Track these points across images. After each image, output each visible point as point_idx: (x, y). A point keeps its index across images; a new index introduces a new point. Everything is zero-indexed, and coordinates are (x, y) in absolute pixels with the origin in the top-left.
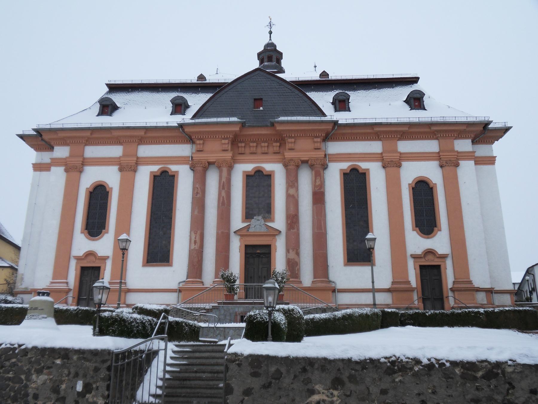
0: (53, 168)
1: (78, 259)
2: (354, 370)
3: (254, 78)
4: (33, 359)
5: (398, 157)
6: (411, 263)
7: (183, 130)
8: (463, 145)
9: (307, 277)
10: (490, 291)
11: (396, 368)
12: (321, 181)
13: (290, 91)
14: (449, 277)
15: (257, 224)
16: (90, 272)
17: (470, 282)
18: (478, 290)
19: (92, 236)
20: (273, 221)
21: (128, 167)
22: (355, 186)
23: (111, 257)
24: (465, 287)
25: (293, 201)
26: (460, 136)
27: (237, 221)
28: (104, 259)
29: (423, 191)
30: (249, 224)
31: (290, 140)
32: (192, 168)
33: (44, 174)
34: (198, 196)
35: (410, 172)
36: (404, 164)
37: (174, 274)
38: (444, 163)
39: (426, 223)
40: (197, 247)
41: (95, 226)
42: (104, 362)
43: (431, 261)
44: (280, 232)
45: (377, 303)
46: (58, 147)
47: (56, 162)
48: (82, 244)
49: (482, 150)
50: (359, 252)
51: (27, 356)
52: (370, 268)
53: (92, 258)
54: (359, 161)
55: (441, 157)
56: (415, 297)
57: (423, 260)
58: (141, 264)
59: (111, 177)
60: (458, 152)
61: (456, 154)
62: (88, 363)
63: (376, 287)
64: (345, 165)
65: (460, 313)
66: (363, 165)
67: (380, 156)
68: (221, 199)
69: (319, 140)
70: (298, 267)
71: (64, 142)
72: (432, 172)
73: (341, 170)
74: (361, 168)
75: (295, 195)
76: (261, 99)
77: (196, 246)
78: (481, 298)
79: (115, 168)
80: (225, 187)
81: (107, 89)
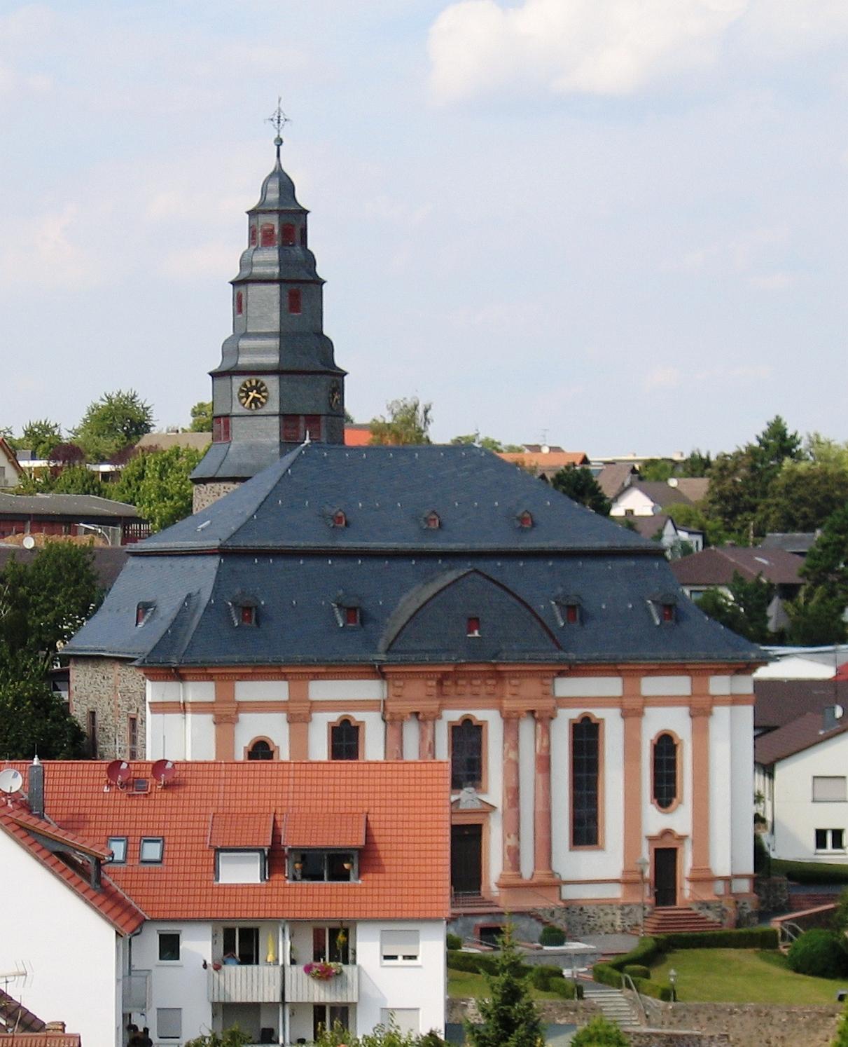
1: (651, 839)
14: (686, 863)
15: (466, 796)
16: (665, 858)
17: (709, 870)
20: (486, 792)
22: (586, 737)
23: (691, 836)
28: (682, 838)
29: (665, 747)
35: (656, 722)
36: (648, 710)
39: (665, 793)
44: (494, 808)
46: (214, 686)
50: (585, 832)
53: (668, 838)
58: (568, 850)
66: (357, 716)
67: (618, 700)
72: (677, 721)
74: (594, 716)
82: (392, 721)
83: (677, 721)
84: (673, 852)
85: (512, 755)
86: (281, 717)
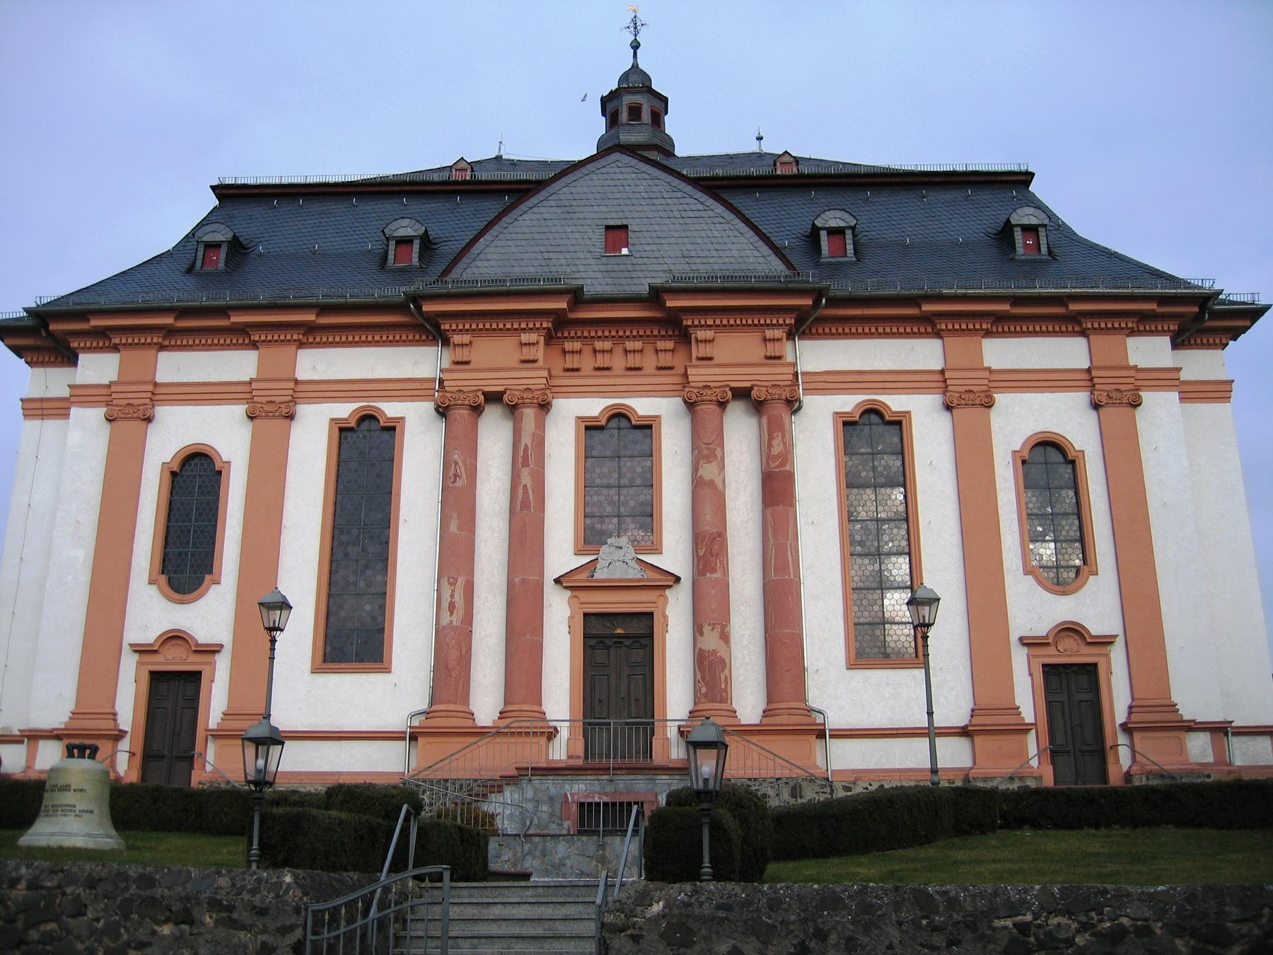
0: (74, 411)
1: (142, 650)
2: (928, 947)
3: (604, 170)
4: (101, 924)
5: (544, 381)
6: (1019, 658)
7: (419, 308)
8: (1150, 351)
9: (748, 702)
10: (1220, 730)
11: (1032, 939)
12: (785, 444)
13: (700, 207)
16: (173, 690)
18: (1193, 727)
19: (176, 590)
20: (657, 550)
21: (271, 409)
24: (1159, 719)
25: (707, 495)
26: (814, 331)
27: (561, 553)
28: (212, 650)
30: (593, 557)
31: (701, 334)
32: (443, 411)
33: (52, 425)
34: (459, 483)
35: (1016, 420)
37: (393, 694)
38: (1104, 399)
40: (456, 619)
41: (186, 564)
42: (284, 931)
43: (174, 660)
44: (678, 579)
45: (941, 764)
47: (84, 395)
48: (150, 613)
49: (1200, 364)
51: (84, 914)
52: (920, 673)
54: (885, 390)
55: (1096, 381)
56: (1032, 749)
57: (1052, 650)
59: (226, 433)
60: (990, 370)
61: (1132, 373)
62: (242, 934)
63: (939, 721)
64: (849, 403)
65: (1014, 793)
68: (521, 491)
69: (778, 333)
70: (726, 672)
71: (103, 340)
72: (1069, 417)
73: (580, 419)
75: (718, 482)
76: (625, 227)
77: (454, 618)
78: (1199, 748)
79: (238, 411)
80: (528, 461)
81: (214, 202)
82: (1113, 401)
83: (1069, 417)
84: (1089, 672)
85: (708, 471)
86: (1080, 398)
